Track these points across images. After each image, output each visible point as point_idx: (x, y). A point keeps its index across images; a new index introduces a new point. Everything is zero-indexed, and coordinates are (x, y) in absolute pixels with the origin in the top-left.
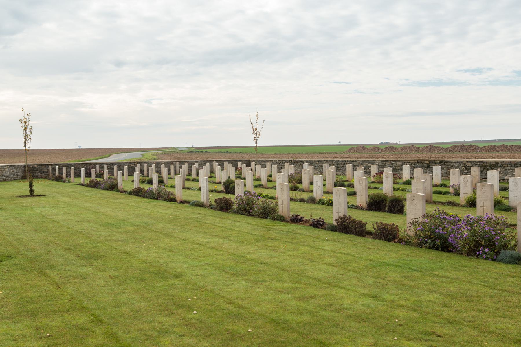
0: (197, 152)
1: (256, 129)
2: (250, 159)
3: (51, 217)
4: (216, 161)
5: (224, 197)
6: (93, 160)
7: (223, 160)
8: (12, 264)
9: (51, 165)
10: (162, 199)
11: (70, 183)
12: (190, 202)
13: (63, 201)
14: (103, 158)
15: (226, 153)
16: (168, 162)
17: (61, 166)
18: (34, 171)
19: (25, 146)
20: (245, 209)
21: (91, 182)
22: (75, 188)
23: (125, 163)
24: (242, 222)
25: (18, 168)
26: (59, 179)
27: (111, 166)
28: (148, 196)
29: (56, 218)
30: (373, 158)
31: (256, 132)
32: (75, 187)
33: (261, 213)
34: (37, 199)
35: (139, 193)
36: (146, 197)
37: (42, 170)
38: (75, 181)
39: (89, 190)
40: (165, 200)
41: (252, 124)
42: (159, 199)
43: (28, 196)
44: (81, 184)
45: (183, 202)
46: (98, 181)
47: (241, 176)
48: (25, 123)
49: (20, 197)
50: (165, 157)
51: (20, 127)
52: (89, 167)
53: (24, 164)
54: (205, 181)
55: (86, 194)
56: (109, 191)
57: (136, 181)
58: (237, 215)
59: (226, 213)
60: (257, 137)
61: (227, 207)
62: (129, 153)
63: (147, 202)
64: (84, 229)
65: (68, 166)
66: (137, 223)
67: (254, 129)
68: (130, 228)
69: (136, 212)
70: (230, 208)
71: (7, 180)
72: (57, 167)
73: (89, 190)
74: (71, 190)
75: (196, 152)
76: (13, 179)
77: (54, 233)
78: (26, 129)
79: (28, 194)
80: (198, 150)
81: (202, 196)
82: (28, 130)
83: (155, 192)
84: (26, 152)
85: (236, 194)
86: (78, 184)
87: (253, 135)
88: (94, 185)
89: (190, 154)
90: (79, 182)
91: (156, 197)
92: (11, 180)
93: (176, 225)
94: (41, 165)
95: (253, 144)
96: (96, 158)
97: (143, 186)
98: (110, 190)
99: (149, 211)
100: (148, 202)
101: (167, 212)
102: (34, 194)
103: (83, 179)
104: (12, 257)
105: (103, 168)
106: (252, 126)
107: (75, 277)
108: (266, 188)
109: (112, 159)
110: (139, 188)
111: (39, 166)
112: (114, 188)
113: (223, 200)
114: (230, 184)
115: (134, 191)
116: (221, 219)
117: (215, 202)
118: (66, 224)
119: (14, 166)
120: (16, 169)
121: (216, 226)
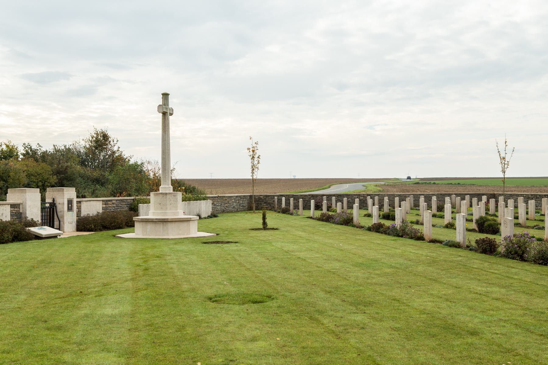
0: (424, 184)
1: (504, 158)
2: (495, 193)
3: (296, 253)
4: (455, 194)
5: (486, 237)
6: (313, 191)
7: (464, 193)
8: (276, 306)
9: (388, 195)
10: (408, 237)
11: (299, 216)
12: (443, 242)
13: (300, 236)
14: (323, 189)
15: (457, 185)
16: (401, 195)
17: (288, 198)
18: (260, 202)
19: (253, 176)
20: (516, 253)
21: (323, 215)
22: (307, 222)
23: (354, 195)
24: (518, 268)
25: (244, 199)
26: (286, 211)
27: (339, 198)
28: (391, 232)
29: (302, 255)
30: (509, 192)
31: (503, 162)
32: (305, 220)
33: (539, 257)
34: (272, 233)
35: (379, 229)
36: (389, 234)
37: (267, 201)
38: (303, 214)
39: (322, 225)
40: (412, 238)
41: (499, 152)
42: (404, 236)
43: (261, 229)
44: (311, 218)
45: (433, 241)
46: (331, 214)
47: (488, 212)
48: (253, 151)
49: (253, 229)
50: (390, 189)
51: (247, 155)
52: (319, 200)
53: (249, 194)
54: (462, 219)
55: (321, 229)
56: (344, 226)
57: (375, 216)
58: (507, 260)
59: (492, 256)
60: (506, 167)
61: (491, 249)
62: (350, 184)
63: (392, 240)
64: (336, 269)
65: (296, 198)
66: (393, 265)
67: (502, 158)
68: (388, 270)
69: (385, 251)
70: (495, 251)
71: (233, 211)
72: (284, 199)
73: (322, 225)
74: (303, 223)
75: (422, 183)
76: (239, 210)
77: (306, 272)
78: (253, 158)
79: (261, 227)
80: (426, 182)
81: (458, 235)
82: (256, 159)
83: (398, 229)
84: (254, 182)
85: (503, 235)
86: (308, 218)
87: (500, 165)
88: (326, 219)
89: (416, 185)
90: (308, 215)
91: (400, 235)
92: (237, 211)
93: (439, 269)
94: (267, 196)
95: (501, 175)
96: (317, 189)
97: (383, 222)
98: (345, 225)
99: (400, 251)
100: (393, 240)
101: (420, 252)
102: (267, 227)
103: (312, 212)
104: (272, 298)
105: (331, 200)
106: (500, 155)
107: (353, 327)
108: (525, 228)
109: (333, 191)
110: (379, 223)
111: (265, 197)
112: (349, 223)
113: (486, 241)
114: (484, 222)
115: (374, 227)
116: (489, 264)
117: (476, 242)
118: (314, 262)
119: (240, 196)
120: (242, 200)
121: (487, 271)
